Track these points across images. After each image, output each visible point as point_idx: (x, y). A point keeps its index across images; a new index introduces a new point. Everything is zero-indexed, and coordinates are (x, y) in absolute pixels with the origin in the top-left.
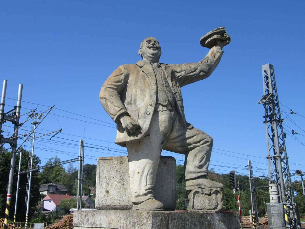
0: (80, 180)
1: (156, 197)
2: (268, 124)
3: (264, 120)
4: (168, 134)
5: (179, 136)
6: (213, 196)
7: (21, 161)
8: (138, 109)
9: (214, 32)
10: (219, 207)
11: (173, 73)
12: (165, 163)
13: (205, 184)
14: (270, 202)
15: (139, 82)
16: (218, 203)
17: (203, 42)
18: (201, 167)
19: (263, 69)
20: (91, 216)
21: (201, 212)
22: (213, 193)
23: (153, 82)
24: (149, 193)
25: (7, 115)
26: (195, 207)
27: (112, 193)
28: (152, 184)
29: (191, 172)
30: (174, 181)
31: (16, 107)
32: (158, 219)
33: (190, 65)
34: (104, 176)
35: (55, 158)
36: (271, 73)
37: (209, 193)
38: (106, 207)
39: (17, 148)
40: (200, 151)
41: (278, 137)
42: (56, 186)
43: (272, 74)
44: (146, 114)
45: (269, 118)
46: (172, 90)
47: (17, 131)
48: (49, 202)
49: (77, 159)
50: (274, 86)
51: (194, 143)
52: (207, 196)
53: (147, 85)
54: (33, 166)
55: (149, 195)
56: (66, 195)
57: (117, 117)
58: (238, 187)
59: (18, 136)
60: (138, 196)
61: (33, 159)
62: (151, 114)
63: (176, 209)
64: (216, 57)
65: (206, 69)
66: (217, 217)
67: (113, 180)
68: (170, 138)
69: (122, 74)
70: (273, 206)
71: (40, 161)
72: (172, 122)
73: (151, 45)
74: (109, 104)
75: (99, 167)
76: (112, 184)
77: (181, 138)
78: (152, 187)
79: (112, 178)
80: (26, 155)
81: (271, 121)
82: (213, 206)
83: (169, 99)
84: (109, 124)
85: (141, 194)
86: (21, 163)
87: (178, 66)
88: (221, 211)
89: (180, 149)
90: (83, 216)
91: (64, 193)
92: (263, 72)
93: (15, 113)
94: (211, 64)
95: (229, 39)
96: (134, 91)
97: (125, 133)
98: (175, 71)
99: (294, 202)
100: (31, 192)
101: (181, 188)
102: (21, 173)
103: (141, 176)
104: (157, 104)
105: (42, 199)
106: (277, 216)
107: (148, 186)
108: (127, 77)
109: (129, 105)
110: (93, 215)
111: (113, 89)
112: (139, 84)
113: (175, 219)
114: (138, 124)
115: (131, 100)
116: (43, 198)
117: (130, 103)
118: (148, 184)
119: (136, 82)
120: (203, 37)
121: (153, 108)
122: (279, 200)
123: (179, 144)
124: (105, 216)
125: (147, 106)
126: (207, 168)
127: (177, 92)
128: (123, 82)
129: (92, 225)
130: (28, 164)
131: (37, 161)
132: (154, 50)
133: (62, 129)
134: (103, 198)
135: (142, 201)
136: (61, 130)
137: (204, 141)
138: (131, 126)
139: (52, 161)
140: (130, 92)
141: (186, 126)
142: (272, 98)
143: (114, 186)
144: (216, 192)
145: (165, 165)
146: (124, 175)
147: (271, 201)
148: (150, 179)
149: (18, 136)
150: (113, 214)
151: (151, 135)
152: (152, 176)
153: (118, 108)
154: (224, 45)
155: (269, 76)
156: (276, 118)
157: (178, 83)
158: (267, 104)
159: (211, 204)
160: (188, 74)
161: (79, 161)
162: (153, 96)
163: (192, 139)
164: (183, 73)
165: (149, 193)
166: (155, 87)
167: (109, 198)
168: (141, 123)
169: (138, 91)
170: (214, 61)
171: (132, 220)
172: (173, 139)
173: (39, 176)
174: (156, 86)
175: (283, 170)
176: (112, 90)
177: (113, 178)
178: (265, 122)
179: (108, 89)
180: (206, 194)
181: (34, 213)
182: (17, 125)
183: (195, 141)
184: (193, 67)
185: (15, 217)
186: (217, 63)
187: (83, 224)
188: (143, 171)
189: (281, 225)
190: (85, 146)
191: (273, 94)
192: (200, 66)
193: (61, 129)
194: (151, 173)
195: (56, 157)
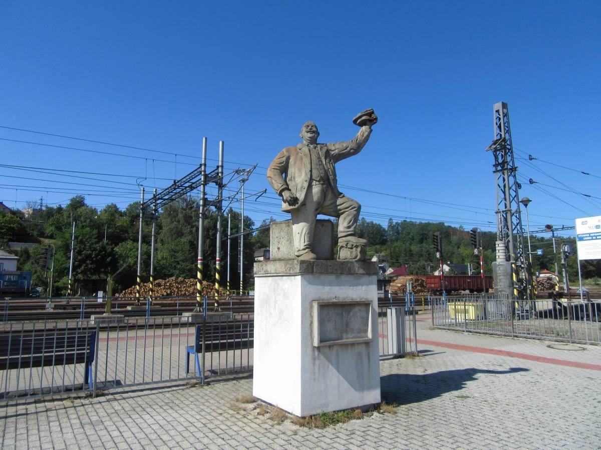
1: (313, 251)
2: (499, 174)
3: (494, 169)
4: (322, 203)
5: (331, 204)
6: (354, 249)
7: (231, 224)
10: (358, 257)
11: (328, 151)
12: (323, 225)
14: (496, 261)
15: (297, 163)
17: (355, 122)
18: (349, 227)
19: (495, 109)
24: (307, 248)
25: (209, 175)
26: (340, 257)
29: (341, 232)
31: (218, 167)
32: (305, 266)
34: (275, 237)
35: (270, 218)
36: (503, 113)
37: (351, 247)
39: (223, 211)
40: (348, 215)
41: (510, 188)
43: (505, 115)
47: (222, 192)
50: (507, 129)
54: (244, 229)
55: (307, 250)
58: (481, 247)
59: (223, 198)
60: (299, 250)
61: (244, 221)
62: (306, 188)
66: (357, 265)
67: (282, 240)
70: (500, 265)
71: (253, 224)
74: (274, 182)
77: (333, 206)
80: (235, 216)
81: (503, 169)
82: (353, 257)
85: (301, 249)
86: (230, 226)
88: (359, 260)
89: (333, 214)
92: (494, 111)
93: (218, 174)
95: (376, 119)
97: (287, 204)
99: (526, 261)
100: (243, 258)
101: (422, 249)
102: (231, 237)
103: (301, 236)
104: (311, 180)
106: (504, 275)
107: (306, 243)
108: (288, 158)
110: (266, 265)
111: (277, 169)
112: (297, 165)
113: (319, 265)
114: (295, 196)
117: (291, 180)
118: (306, 241)
119: (295, 163)
120: (354, 119)
121: (308, 183)
122: (508, 259)
123: (332, 210)
130: (238, 227)
131: (248, 223)
136: (266, 190)
137: (352, 207)
138: (290, 198)
140: (291, 170)
141: (339, 195)
142: (503, 143)
143: (283, 243)
144: (357, 247)
147: (497, 260)
148: (307, 238)
149: (223, 198)
152: (308, 235)
154: (372, 125)
155: (501, 117)
156: (507, 167)
157: (332, 160)
158: (498, 150)
163: (342, 206)
164: (337, 151)
165: (307, 248)
166: (309, 166)
168: (298, 196)
169: (296, 170)
173: (253, 241)
175: (514, 227)
176: (276, 171)
178: (494, 172)
181: (249, 281)
182: (221, 186)
183: (345, 207)
184: (345, 145)
185: (228, 284)
188: (302, 232)
189: (508, 285)
191: (505, 138)
192: (350, 144)
194: (308, 233)
195: (271, 217)
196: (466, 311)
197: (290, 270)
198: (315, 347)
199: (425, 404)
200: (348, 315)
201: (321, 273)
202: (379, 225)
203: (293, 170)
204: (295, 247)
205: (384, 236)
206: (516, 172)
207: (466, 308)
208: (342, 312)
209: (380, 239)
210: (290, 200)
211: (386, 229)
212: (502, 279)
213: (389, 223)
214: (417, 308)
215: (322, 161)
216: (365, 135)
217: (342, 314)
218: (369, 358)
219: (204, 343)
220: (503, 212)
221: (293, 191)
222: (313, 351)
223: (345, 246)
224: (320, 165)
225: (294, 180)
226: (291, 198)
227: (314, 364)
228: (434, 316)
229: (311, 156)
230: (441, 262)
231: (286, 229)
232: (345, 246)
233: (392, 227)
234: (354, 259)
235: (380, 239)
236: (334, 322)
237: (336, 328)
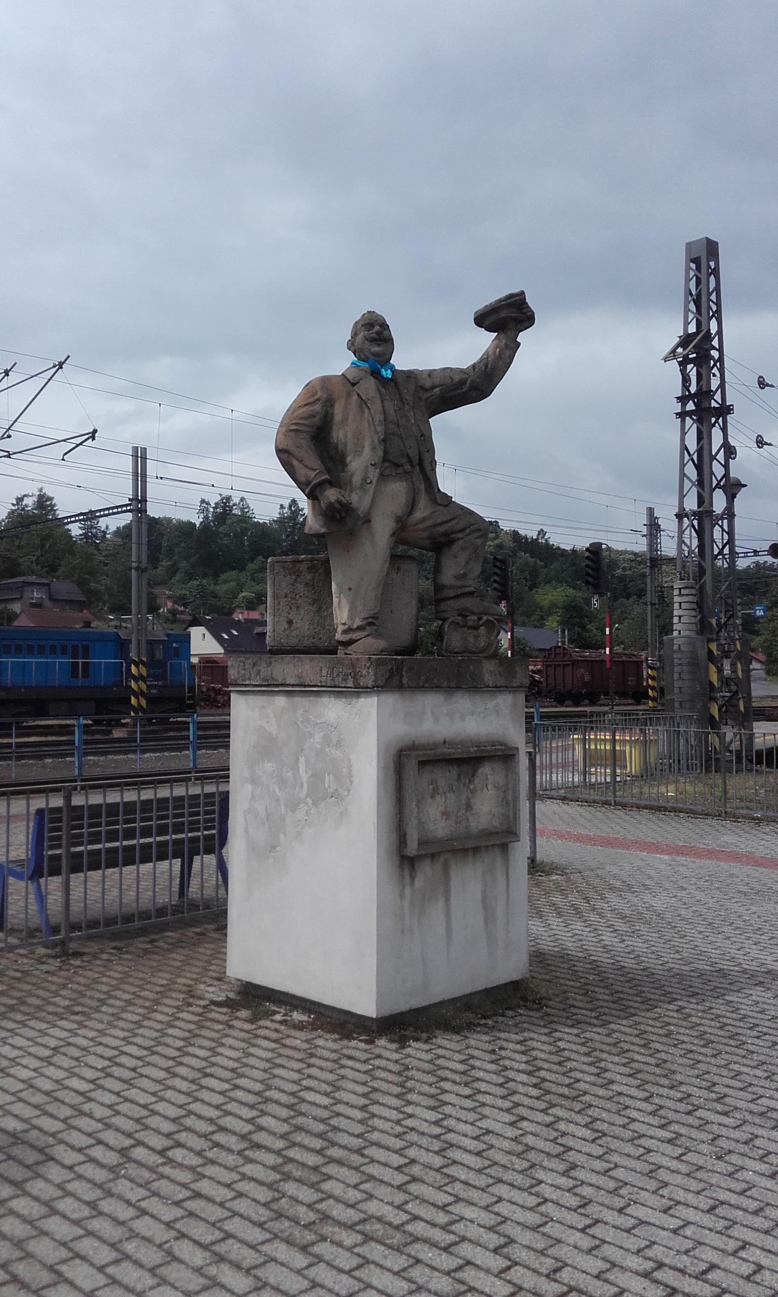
3: (678, 408)
12: (399, 568)
20: (265, 665)
24: (370, 624)
42: (48, 585)
45: (694, 402)
49: (126, 505)
85: (355, 626)
124: (291, 666)
136: (95, 431)
139: (26, 506)
151: (373, 519)
153: (311, 472)
172: (415, 525)
179: (292, 434)
187: (249, 679)
193: (135, 456)
196: (618, 754)
197: (345, 680)
199: (150, 963)
206: (729, 417)
207: (618, 748)
212: (477, 637)
219: (68, 850)
220: (694, 514)
227: (402, 896)
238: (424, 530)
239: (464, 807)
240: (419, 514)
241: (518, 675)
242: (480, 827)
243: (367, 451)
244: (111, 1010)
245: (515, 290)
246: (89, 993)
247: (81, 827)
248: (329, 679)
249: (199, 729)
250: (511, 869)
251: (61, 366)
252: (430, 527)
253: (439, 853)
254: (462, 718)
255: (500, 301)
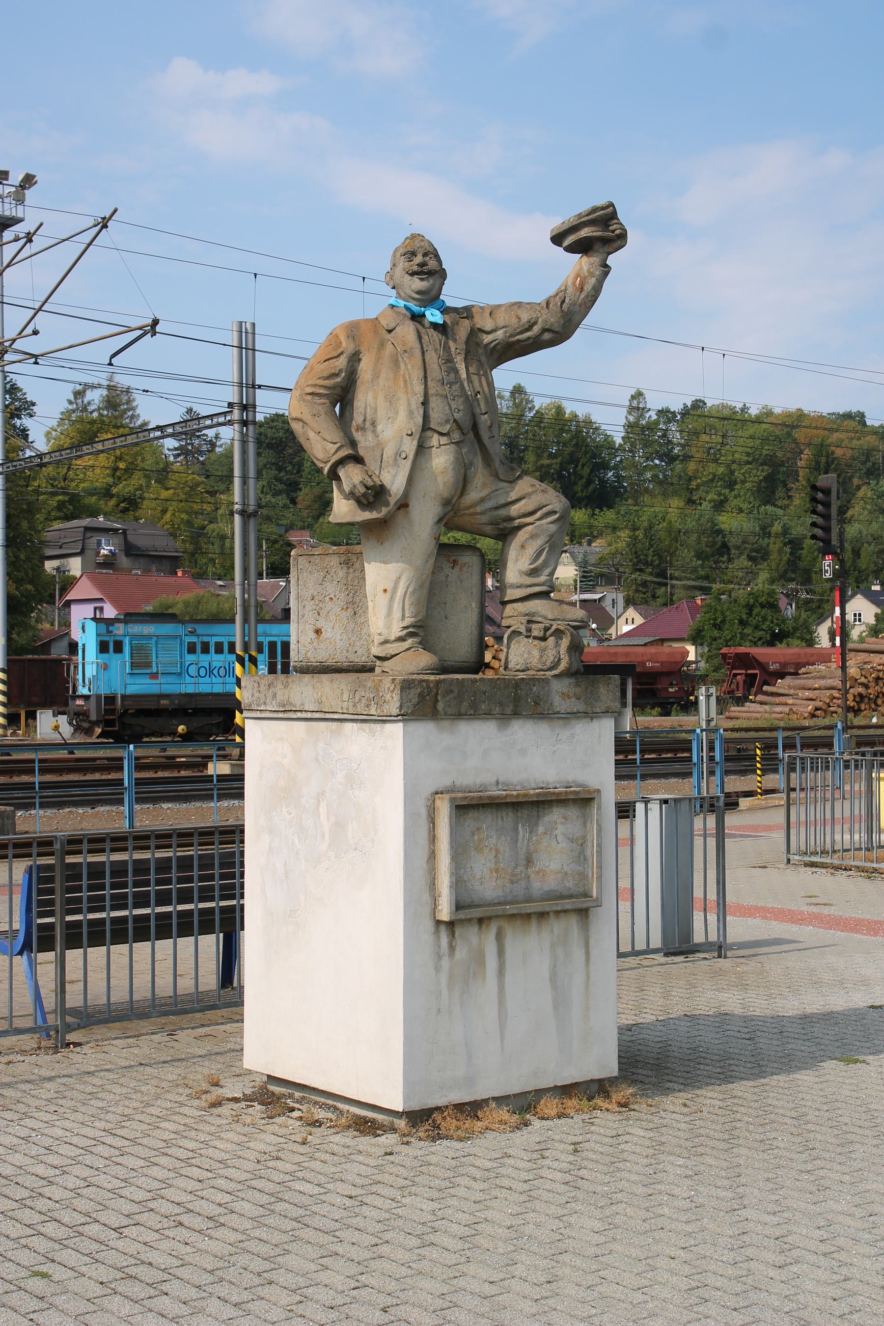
0: (242, 513)
1: (425, 645)
6: (551, 640)
8: (380, 444)
9: (583, 219)
13: (544, 613)
15: (383, 376)
16: (562, 656)
21: (521, 675)
22: (551, 636)
23: (416, 374)
24: (411, 635)
26: (511, 665)
27: (329, 635)
28: (415, 617)
30: (474, 605)
32: (414, 694)
33: (519, 313)
34: (308, 595)
37: (541, 634)
38: (317, 666)
40: (533, 536)
44: (398, 457)
46: (467, 388)
48: (95, 609)
49: (225, 414)
51: (519, 518)
52: (536, 642)
53: (402, 384)
56: (176, 573)
57: (331, 467)
60: (386, 642)
62: (411, 457)
63: (699, 648)
64: (585, 288)
65: (556, 324)
68: (462, 506)
69: (342, 353)
72: (463, 470)
73: (415, 268)
74: (312, 435)
75: (296, 573)
76: (328, 612)
78: (416, 622)
79: (327, 598)
82: (548, 664)
83: (455, 415)
84: (364, 278)
85: (393, 638)
87: (488, 315)
88: (568, 673)
90: (262, 688)
91: (171, 563)
94: (571, 309)
96: (370, 397)
98: (481, 330)
103: (392, 599)
104: (426, 427)
105: (61, 596)
107: (408, 621)
108: (355, 358)
109: (360, 433)
112: (382, 381)
113: (452, 691)
115: (365, 420)
116: (64, 590)
117: (361, 428)
119: (376, 376)
121: (415, 443)
124: (310, 687)
125: (402, 437)
126: (552, 573)
127: (479, 392)
128: (343, 374)
129: (284, 706)
132: (422, 279)
133: (158, 323)
134: (307, 645)
135: (393, 653)
136: (156, 322)
137: (545, 510)
138: (362, 490)
143: (332, 617)
144: (558, 633)
145: (453, 568)
146: (356, 592)
150: (327, 683)
153: (332, 445)
159: (544, 659)
160: (512, 336)
161: (236, 426)
162: (416, 412)
164: (500, 334)
166: (419, 389)
167: (322, 646)
169: (381, 398)
170: (580, 301)
171: (363, 694)
174: (423, 387)
176: (318, 400)
177: (331, 598)
179: (309, 397)
180: (535, 638)
186: (588, 304)
188: (395, 588)
190: (260, 387)
197: (368, 706)
198: (438, 923)
200: (531, 833)
201: (459, 715)
202: (589, 422)
203: (370, 397)
204: (373, 630)
205: (605, 466)
208: (517, 824)
209: (589, 482)
210: (364, 495)
211: (618, 441)
213: (631, 409)
214: (735, 783)
215: (456, 371)
216: (588, 287)
217: (516, 830)
218: (587, 953)
221: (372, 464)
222: (437, 932)
223: (523, 629)
224: (451, 384)
225: (374, 431)
226: (367, 488)
227: (438, 969)
228: (793, 819)
229: (423, 353)
230: (837, 594)
231: (341, 574)
232: (523, 629)
233: (643, 428)
234: (550, 669)
235: (589, 482)
236: (494, 854)
237: (497, 871)
238: (482, 513)
239: (524, 862)
240: (473, 495)
241: (603, 698)
242: (546, 888)
243: (402, 415)
244: (100, 1104)
245: (601, 202)
246: (138, 1117)
247: (79, 889)
248: (351, 704)
249: (139, 767)
250: (592, 942)
251: (104, 224)
252: (491, 509)
253: (490, 918)
254: (523, 752)
255: (580, 216)
